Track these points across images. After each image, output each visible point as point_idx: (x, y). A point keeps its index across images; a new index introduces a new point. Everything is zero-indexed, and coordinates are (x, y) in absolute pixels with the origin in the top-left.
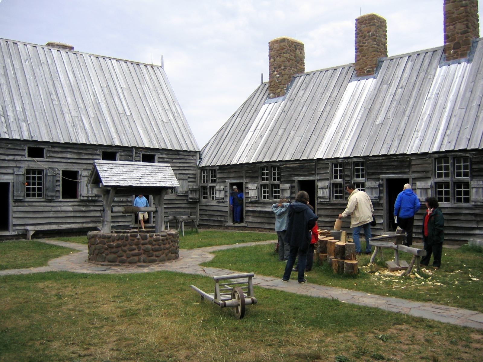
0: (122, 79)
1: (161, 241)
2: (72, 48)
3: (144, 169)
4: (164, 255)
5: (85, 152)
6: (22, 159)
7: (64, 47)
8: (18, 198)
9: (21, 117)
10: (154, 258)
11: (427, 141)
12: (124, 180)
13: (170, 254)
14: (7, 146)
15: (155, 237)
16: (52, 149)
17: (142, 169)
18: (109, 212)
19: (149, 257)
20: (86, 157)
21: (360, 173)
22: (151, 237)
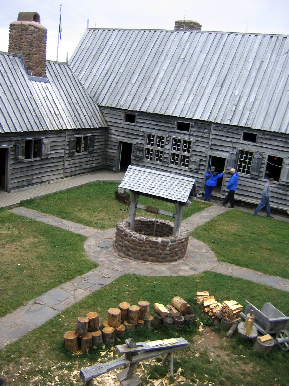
4: (139, 255)
6: (238, 142)
9: (249, 106)
14: (228, 130)
16: (263, 137)
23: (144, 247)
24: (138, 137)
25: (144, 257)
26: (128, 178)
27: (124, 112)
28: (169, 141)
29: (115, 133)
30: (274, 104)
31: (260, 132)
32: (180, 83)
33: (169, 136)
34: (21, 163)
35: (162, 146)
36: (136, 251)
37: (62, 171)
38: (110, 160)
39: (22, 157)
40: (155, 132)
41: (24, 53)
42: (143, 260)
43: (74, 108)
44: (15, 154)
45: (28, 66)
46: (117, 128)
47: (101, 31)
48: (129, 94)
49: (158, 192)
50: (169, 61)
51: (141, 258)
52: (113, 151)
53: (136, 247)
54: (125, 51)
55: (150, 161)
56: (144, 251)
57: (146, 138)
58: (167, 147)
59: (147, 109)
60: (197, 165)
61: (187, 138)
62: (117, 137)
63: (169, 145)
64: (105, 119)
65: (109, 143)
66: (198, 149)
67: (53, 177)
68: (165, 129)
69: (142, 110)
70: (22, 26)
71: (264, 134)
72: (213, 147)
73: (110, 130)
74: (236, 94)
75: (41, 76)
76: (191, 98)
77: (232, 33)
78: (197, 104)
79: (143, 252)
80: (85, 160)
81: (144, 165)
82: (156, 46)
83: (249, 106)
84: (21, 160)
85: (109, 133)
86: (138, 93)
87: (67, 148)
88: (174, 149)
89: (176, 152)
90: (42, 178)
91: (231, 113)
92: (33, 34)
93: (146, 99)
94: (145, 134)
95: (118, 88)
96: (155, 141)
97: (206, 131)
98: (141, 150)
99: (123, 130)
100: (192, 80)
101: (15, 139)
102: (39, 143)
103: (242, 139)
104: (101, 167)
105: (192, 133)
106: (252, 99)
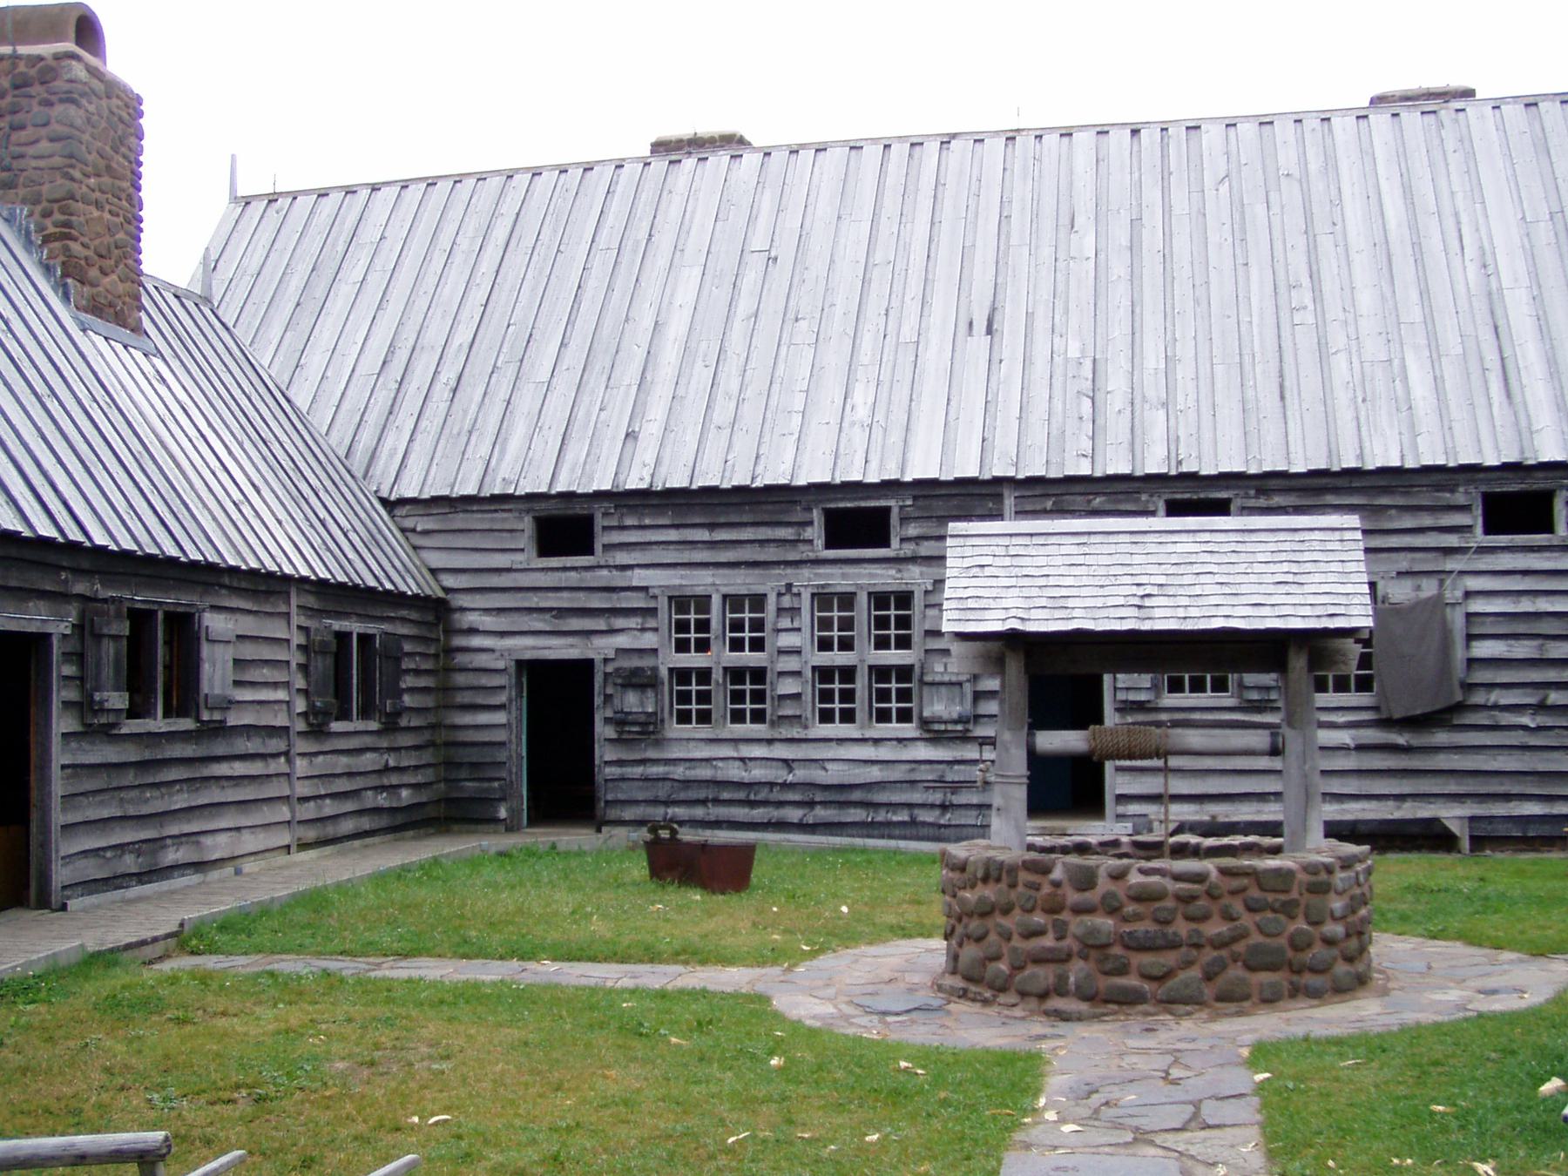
1: (1169, 903)
2: (1468, 94)
3: (1197, 548)
4: (1195, 973)
5: (1400, 501)
7: (1445, 95)
8: (1132, 697)
9: (1153, 389)
10: (1132, 981)
12: (1062, 603)
13: (1236, 972)
14: (1089, 501)
15: (1135, 878)
16: (1262, 502)
17: (1179, 548)
18: (1013, 751)
19: (1107, 973)
20: (1408, 522)
22: (1118, 876)
23: (1216, 918)
24: (620, 623)
25: (1220, 981)
26: (975, 582)
27: (528, 512)
28: (794, 611)
29: (488, 622)
30: (1258, 369)
31: (1247, 483)
32: (783, 350)
33: (789, 586)
34: (107, 733)
35: (757, 645)
36: (1169, 959)
38: (474, 765)
39: (118, 700)
40: (710, 580)
41: (39, 194)
42: (1224, 997)
44: (82, 679)
45: (62, 258)
46: (495, 595)
47: (304, 203)
48: (537, 426)
49: (1193, 612)
50: (698, 271)
51: (1208, 991)
52: (483, 718)
53: (1170, 930)
54: (458, 258)
55: (704, 731)
56: (1219, 943)
57: (665, 616)
58: (786, 640)
59: (653, 476)
60: (962, 695)
61: (887, 579)
62: (499, 642)
63: (799, 630)
64: (423, 562)
65: (461, 679)
67: (250, 842)
68: (762, 557)
69: (632, 484)
70: (15, 66)
73: (457, 616)
74: (1074, 352)
75: (120, 320)
76: (862, 397)
77: (954, 136)
78: (899, 416)
79: (1215, 948)
80: (369, 761)
81: (675, 756)
82: (614, 219)
83: (1153, 389)
84: (112, 719)
85: (451, 631)
86: (581, 414)
87: (300, 683)
90: (203, 839)
91: (1080, 429)
92: (84, 102)
93: (630, 436)
94: (655, 597)
95: (465, 412)
96: (715, 624)
98: (641, 680)
99: (535, 600)
100: (839, 324)
101: (80, 588)
102: (184, 629)
104: (431, 812)
105: (908, 549)
106: (1153, 359)
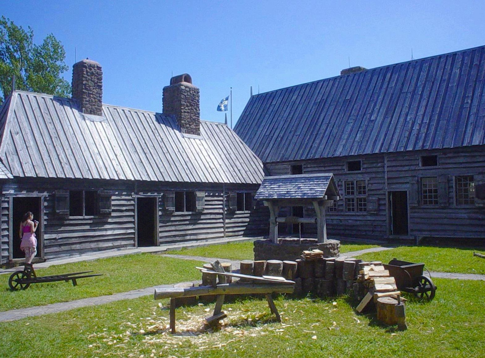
0: (60, 149)
6: (417, 168)
11: (386, 146)
21: (350, 190)
27: (290, 164)
37: (222, 230)
43: (233, 164)
63: (342, 190)
66: (374, 187)
71: (445, 154)
72: (390, 181)
88: (348, 193)
89: (351, 196)
97: (379, 165)
103: (420, 165)
105: (364, 171)
